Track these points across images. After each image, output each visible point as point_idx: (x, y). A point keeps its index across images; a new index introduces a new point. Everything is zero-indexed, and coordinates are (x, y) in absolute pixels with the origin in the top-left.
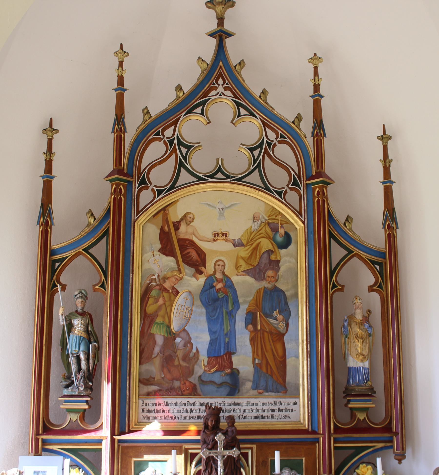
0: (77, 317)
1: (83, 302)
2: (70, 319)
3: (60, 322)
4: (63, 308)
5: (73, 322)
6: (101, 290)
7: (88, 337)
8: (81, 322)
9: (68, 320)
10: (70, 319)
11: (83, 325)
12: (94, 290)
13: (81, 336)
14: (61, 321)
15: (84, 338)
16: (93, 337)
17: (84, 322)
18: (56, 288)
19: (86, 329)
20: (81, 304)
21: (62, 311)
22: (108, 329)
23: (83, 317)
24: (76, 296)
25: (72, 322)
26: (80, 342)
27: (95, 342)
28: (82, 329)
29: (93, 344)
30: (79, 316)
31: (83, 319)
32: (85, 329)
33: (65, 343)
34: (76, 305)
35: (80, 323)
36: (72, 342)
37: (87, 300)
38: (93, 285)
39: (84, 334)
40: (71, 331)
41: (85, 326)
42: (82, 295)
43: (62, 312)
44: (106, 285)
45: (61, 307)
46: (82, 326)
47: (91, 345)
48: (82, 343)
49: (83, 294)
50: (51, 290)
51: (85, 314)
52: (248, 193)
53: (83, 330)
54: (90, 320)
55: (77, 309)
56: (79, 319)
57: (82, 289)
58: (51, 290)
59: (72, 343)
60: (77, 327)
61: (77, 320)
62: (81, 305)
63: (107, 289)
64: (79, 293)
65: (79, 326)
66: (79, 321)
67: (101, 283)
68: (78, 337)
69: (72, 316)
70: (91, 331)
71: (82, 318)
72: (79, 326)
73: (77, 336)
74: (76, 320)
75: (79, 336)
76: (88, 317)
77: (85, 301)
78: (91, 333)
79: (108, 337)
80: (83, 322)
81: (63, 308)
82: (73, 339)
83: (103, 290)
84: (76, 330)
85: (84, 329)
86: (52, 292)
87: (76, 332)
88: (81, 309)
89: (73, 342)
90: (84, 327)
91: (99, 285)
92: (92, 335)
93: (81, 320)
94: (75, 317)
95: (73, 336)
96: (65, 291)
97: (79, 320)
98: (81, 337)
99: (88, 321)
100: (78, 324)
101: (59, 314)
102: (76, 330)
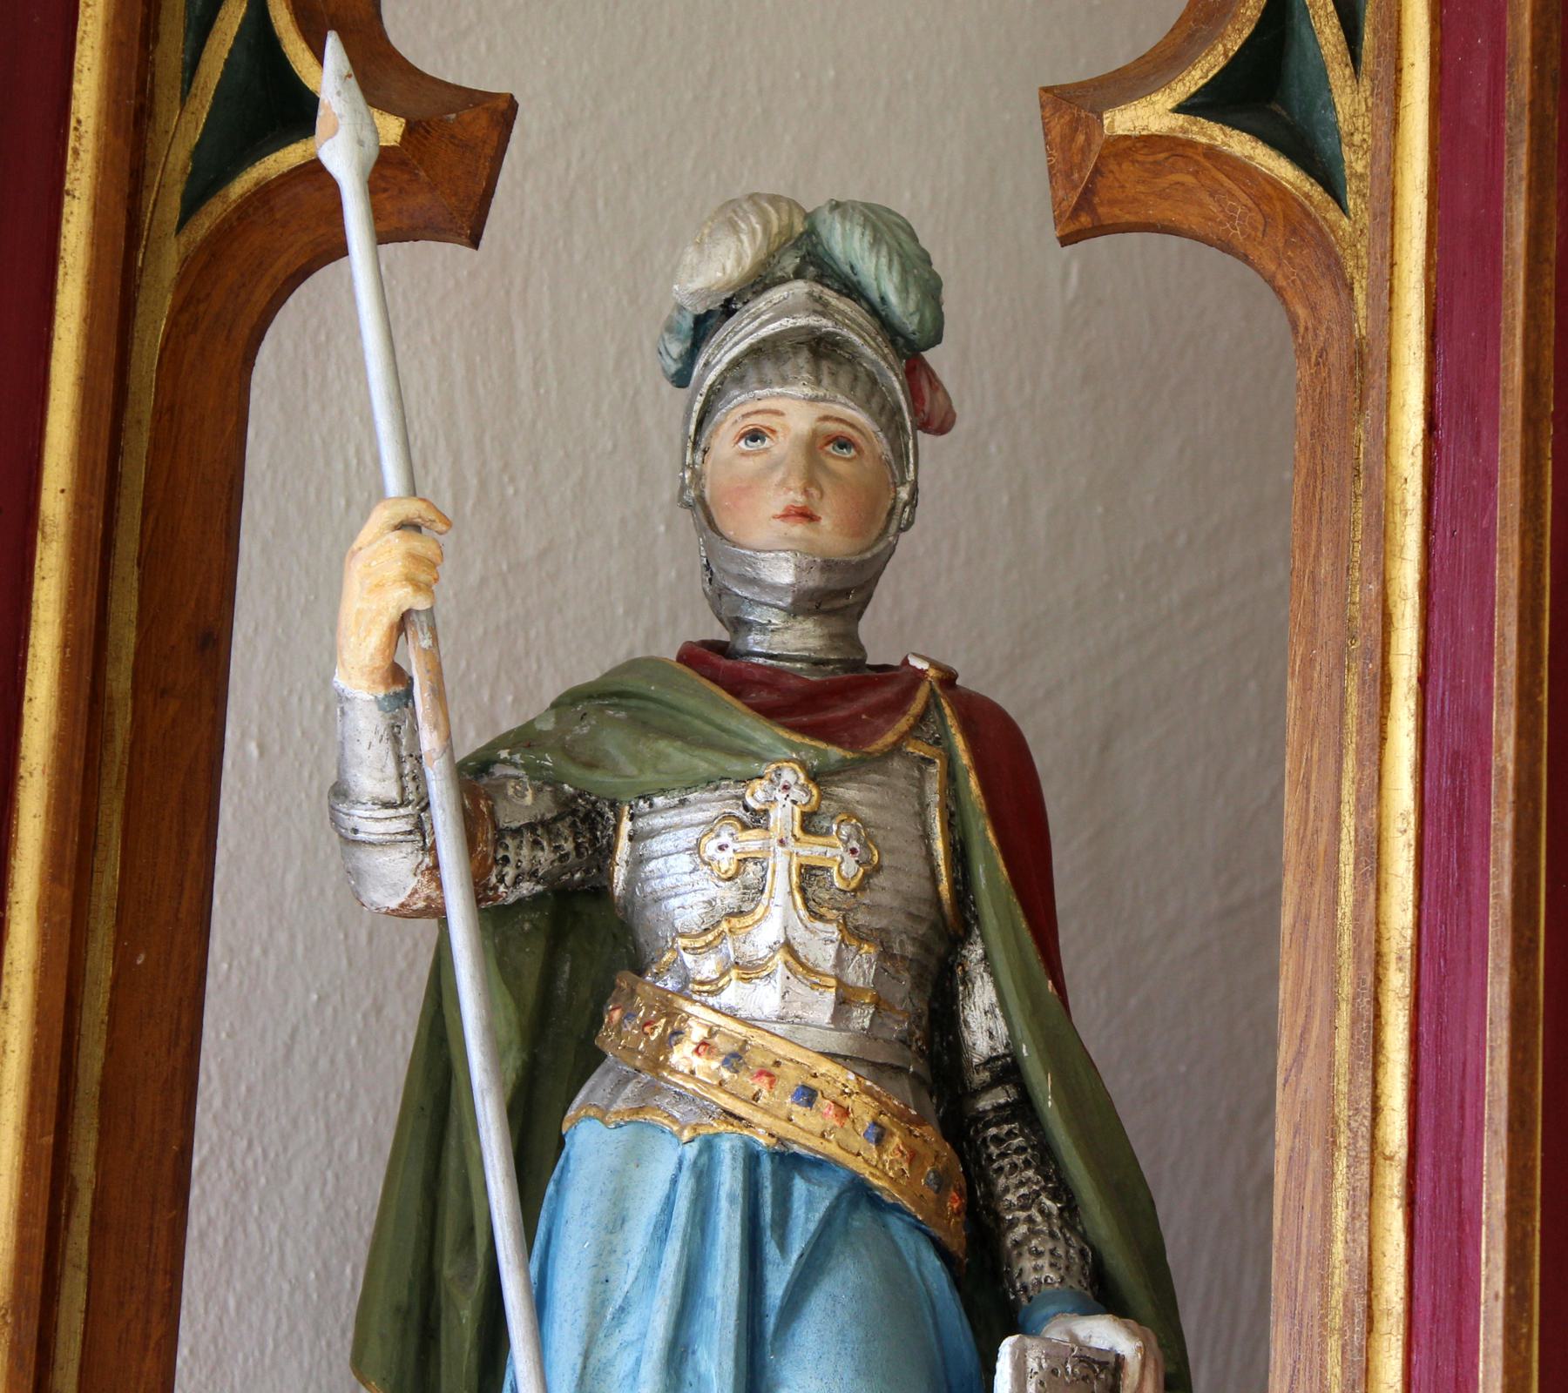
0: (702, 763)
1: (839, 463)
2: (567, 806)
3: (351, 842)
4: (409, 526)
5: (638, 861)
6: (1240, 170)
7: (941, 1182)
8: (812, 850)
9: (539, 829)
10: (567, 806)
11: (853, 933)
12: (1086, 201)
13: (790, 1162)
14: (370, 823)
15: (859, 1193)
16: (1062, 1190)
17: (872, 871)
18: (290, 156)
19: (897, 1027)
20: (810, 482)
21: (401, 597)
22: (1398, 981)
23: (836, 753)
24: (703, 328)
25: (620, 875)
26: (777, 1286)
27: (1087, 1311)
28: (822, 1007)
29: (1055, 1333)
30: (764, 734)
31: (850, 792)
32: (879, 1004)
33: (463, 1316)
34: (704, 514)
35: (781, 884)
36: (601, 1282)
37: (925, 439)
38: (1057, 98)
39: (863, 1108)
40: (598, 1057)
41: (886, 954)
42: (824, 309)
43: (402, 624)
44: (1338, 73)
45: (382, 516)
46: (821, 945)
47: (1007, 1347)
48: (818, 1306)
49: (851, 289)
50: (192, 204)
51: (897, 706)
52: (1381, 1305)
53: (836, 1041)
54: (984, 836)
55: (718, 596)
56: (756, 795)
57: (836, 206)
58: (192, 204)
59: (597, 1309)
60: (707, 967)
61: (710, 827)
62: (806, 515)
63: (1355, 162)
64: (760, 281)
65: (765, 934)
66: (752, 841)
67: (1233, 41)
68: (729, 1179)
69: (614, 742)
70: (1007, 1070)
71: (816, 776)
72: (765, 934)
73: (709, 1146)
74: (706, 807)
75: (752, 1160)
76: (951, 776)
77: (882, 446)
78: (1024, 1109)
79: (1393, 1179)
80: (844, 868)
81: (409, 526)
82: (617, 1221)
83: (1283, 170)
84: (699, 1020)
85: (861, 1018)
86: (225, 234)
87: (682, 1056)
88: (808, 604)
89: (625, 1279)
90: (862, 968)
91: (1195, 78)
92: (1045, 1155)
93: (809, 823)
94: (677, 755)
95: (634, 1157)
96: (474, 242)
97: (757, 819)
98: (799, 1186)
99: (960, 854)
100: (729, 896)
101: (340, 681)
102: (697, 1033)
